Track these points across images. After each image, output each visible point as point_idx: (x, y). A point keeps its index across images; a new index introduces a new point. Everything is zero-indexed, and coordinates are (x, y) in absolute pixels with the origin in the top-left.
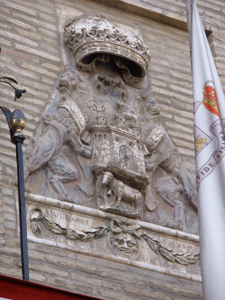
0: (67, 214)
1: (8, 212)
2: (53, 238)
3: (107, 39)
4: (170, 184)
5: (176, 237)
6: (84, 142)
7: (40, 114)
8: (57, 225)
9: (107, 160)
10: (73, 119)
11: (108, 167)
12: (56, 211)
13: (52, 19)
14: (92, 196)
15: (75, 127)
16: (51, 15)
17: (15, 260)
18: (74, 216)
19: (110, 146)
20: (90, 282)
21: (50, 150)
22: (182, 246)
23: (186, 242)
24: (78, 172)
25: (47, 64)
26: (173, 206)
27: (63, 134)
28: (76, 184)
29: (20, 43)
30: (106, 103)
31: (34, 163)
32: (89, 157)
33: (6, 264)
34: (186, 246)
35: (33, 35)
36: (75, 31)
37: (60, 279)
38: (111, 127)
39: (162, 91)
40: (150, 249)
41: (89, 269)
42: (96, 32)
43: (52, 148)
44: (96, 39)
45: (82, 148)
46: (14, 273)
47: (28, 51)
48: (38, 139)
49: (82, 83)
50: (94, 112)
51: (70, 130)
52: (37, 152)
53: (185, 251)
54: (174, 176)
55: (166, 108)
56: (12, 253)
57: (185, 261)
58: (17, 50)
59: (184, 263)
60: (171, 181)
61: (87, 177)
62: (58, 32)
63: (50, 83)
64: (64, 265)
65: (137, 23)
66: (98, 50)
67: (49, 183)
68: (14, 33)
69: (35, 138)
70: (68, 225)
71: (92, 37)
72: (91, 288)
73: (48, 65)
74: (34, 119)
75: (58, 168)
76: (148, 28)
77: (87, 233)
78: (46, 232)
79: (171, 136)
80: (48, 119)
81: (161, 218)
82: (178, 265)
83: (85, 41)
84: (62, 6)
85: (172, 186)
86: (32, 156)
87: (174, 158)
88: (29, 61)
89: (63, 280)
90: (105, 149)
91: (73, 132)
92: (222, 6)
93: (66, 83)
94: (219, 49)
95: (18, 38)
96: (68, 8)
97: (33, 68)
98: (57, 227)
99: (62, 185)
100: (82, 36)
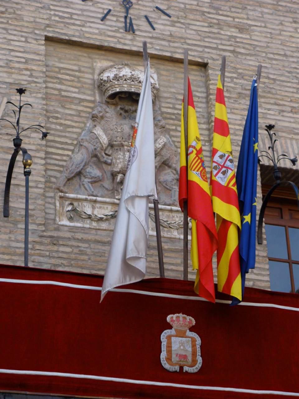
0: (93, 204)
1: (50, 208)
2: (82, 221)
3: (125, 82)
4: (169, 176)
5: (171, 211)
6: (106, 154)
7: (77, 138)
8: (85, 213)
9: (120, 166)
10: (99, 140)
11: (120, 171)
12: (85, 204)
13: (90, 71)
14: (112, 190)
15: (100, 145)
16: (89, 68)
17: (51, 240)
18: (98, 205)
19: (123, 156)
20: (104, 249)
21: (81, 163)
22: (176, 216)
23: (179, 214)
24: (102, 175)
25: (85, 103)
26: (170, 190)
27: (91, 151)
28: (101, 183)
29: (65, 91)
30: (125, 125)
31: (70, 173)
32: (110, 164)
33: (45, 243)
34: (179, 216)
35: (75, 84)
36: (102, 79)
37: (83, 249)
38: (124, 143)
39: (169, 111)
40: (152, 221)
41: (103, 240)
42: (116, 77)
43: (82, 161)
44: (116, 83)
45: (105, 159)
46: (50, 249)
47: (71, 96)
48: (74, 156)
49: (108, 114)
50: (115, 132)
51: (96, 148)
52: (72, 165)
53: (177, 219)
54: (173, 169)
55: (172, 122)
56: (50, 236)
57: (176, 227)
58: (63, 96)
59: (176, 228)
60: (171, 173)
61: (109, 178)
62: (93, 79)
63: (86, 116)
64: (85, 239)
65: (154, 64)
66: (118, 90)
67: (81, 185)
68: (61, 85)
69: (72, 156)
70: (93, 212)
71: (114, 81)
72: (105, 253)
73: (86, 104)
74: (73, 142)
75: (88, 174)
76: (162, 67)
77: (106, 215)
78: (78, 218)
79: (174, 142)
80: (82, 141)
81: (162, 199)
82: (171, 229)
83: (109, 85)
84: (97, 60)
85: (170, 177)
86: (69, 169)
87: (173, 158)
88: (71, 103)
89: (85, 249)
90: (119, 158)
91: (98, 149)
92: (218, 43)
93: (95, 115)
94: (213, 75)
95: (63, 87)
96: (102, 61)
97: (74, 107)
98: (84, 214)
99: (90, 185)
100: (107, 81)
